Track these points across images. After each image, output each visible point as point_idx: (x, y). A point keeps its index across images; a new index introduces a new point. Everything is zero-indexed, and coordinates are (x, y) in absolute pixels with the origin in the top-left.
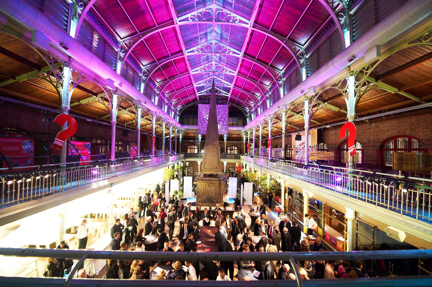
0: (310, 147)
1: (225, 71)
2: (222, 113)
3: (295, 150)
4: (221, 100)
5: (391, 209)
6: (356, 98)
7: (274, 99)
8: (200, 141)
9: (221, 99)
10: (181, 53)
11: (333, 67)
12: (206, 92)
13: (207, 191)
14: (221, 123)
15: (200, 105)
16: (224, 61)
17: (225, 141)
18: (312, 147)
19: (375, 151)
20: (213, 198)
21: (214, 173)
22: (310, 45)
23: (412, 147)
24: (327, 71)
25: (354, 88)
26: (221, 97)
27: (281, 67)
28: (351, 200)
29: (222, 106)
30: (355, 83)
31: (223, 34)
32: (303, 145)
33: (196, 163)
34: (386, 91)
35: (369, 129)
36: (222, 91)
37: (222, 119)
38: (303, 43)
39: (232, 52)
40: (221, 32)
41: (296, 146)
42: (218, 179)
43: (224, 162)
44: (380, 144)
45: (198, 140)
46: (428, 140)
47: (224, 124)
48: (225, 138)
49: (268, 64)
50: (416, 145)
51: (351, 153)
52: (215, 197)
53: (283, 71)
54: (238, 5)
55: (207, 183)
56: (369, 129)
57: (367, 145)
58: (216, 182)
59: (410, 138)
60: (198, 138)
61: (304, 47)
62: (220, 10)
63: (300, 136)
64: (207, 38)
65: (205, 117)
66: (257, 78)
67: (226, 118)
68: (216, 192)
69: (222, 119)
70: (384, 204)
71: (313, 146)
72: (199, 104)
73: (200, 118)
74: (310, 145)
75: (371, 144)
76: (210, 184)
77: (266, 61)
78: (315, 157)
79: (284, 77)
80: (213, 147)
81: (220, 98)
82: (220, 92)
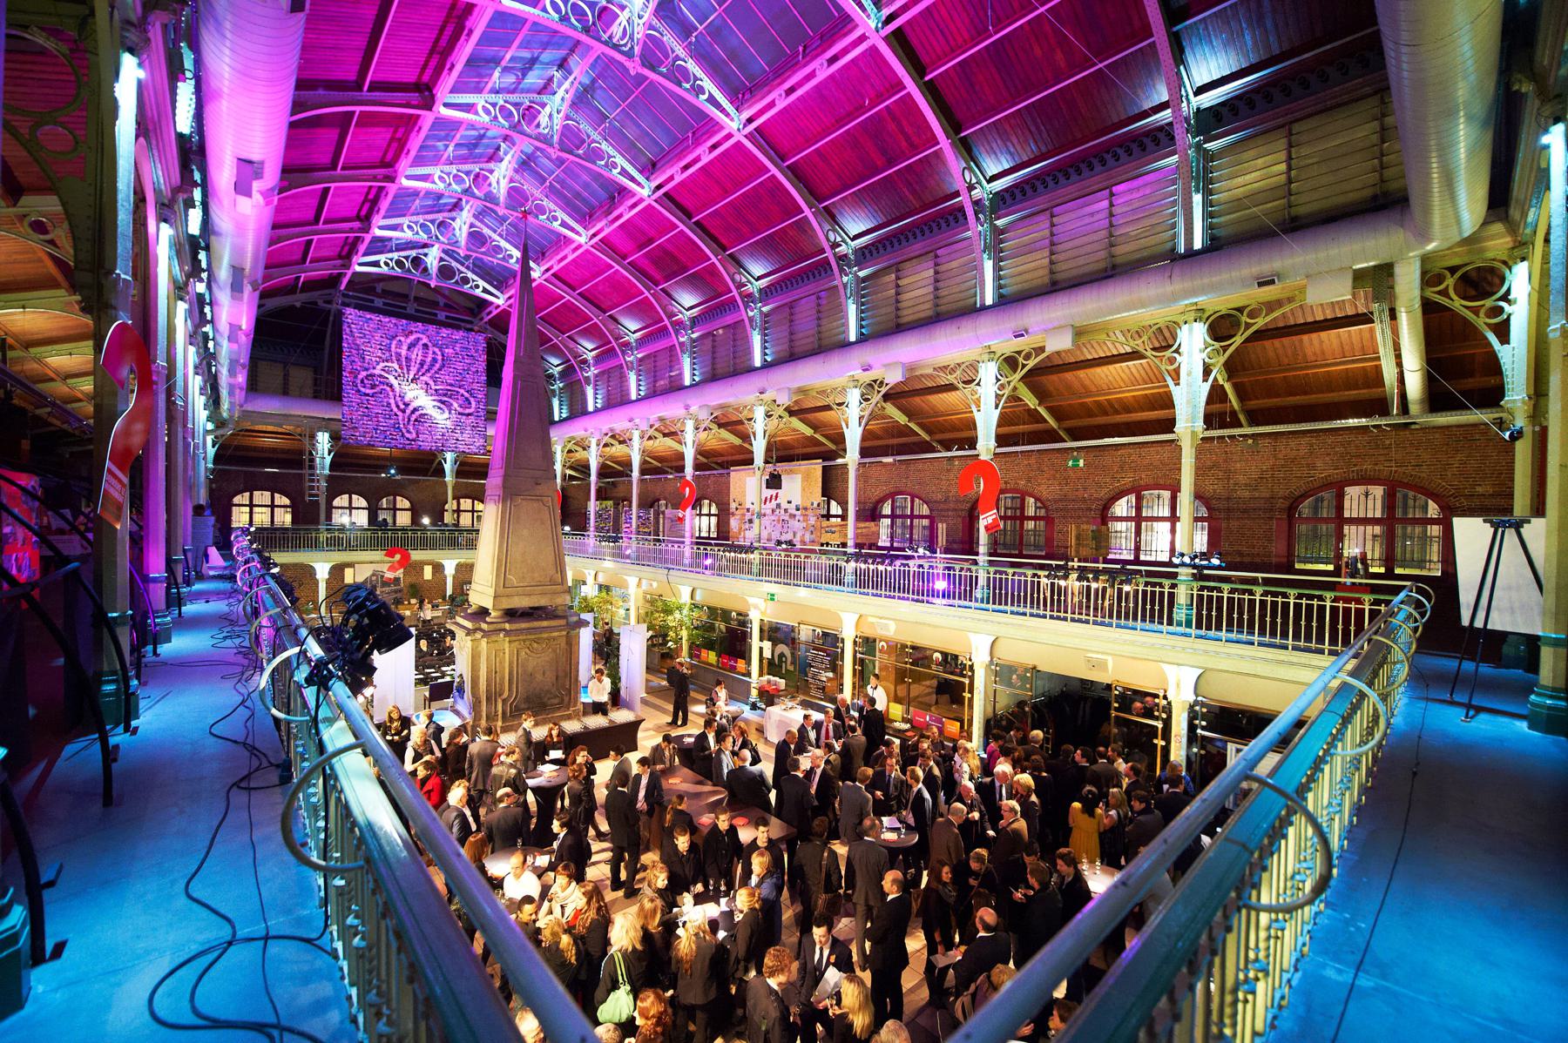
0: (798, 509)
1: (548, 219)
2: (460, 366)
3: (744, 515)
4: (448, 307)
5: (1095, 623)
6: (998, 411)
7: (714, 358)
8: (327, 472)
9: (446, 305)
10: (414, 97)
11: (971, 334)
12: (399, 263)
13: (525, 671)
14: (455, 405)
15: (351, 314)
16: (545, 180)
17: (449, 478)
18: (806, 509)
19: (960, 520)
20: (548, 691)
21: (542, 601)
22: (872, 244)
23: (1377, 529)
24: (955, 338)
25: (996, 388)
26: (444, 296)
27: (757, 269)
28: (1015, 622)
29: (458, 335)
30: (998, 380)
31: (598, 91)
32: (774, 503)
33: (309, 572)
34: (1021, 400)
35: (948, 470)
36: (470, 275)
37: (462, 391)
38: (853, 231)
39: (619, 170)
40: (594, 81)
41: (748, 505)
42: (563, 622)
43: (444, 562)
44: (969, 505)
45: (312, 467)
46: (1056, 501)
47: (467, 411)
48: (448, 467)
49: (725, 250)
50: (1031, 508)
51: (986, 527)
52: (554, 690)
53: (764, 283)
54: (712, 46)
55: (524, 641)
56: (948, 470)
57: (942, 506)
58: (556, 634)
59: (1023, 496)
60: (312, 460)
61: (853, 244)
62: (655, 30)
63: (779, 476)
64: (524, 75)
65: (377, 371)
66: (658, 276)
67: (475, 386)
68: (557, 670)
69: (462, 391)
70: (1084, 617)
71: (809, 505)
72: (349, 310)
73: (354, 373)
74: (799, 503)
75: (952, 505)
76: (535, 645)
77: (720, 238)
78: (836, 535)
79: (763, 300)
80: (536, 505)
81: (442, 301)
82: (466, 280)
